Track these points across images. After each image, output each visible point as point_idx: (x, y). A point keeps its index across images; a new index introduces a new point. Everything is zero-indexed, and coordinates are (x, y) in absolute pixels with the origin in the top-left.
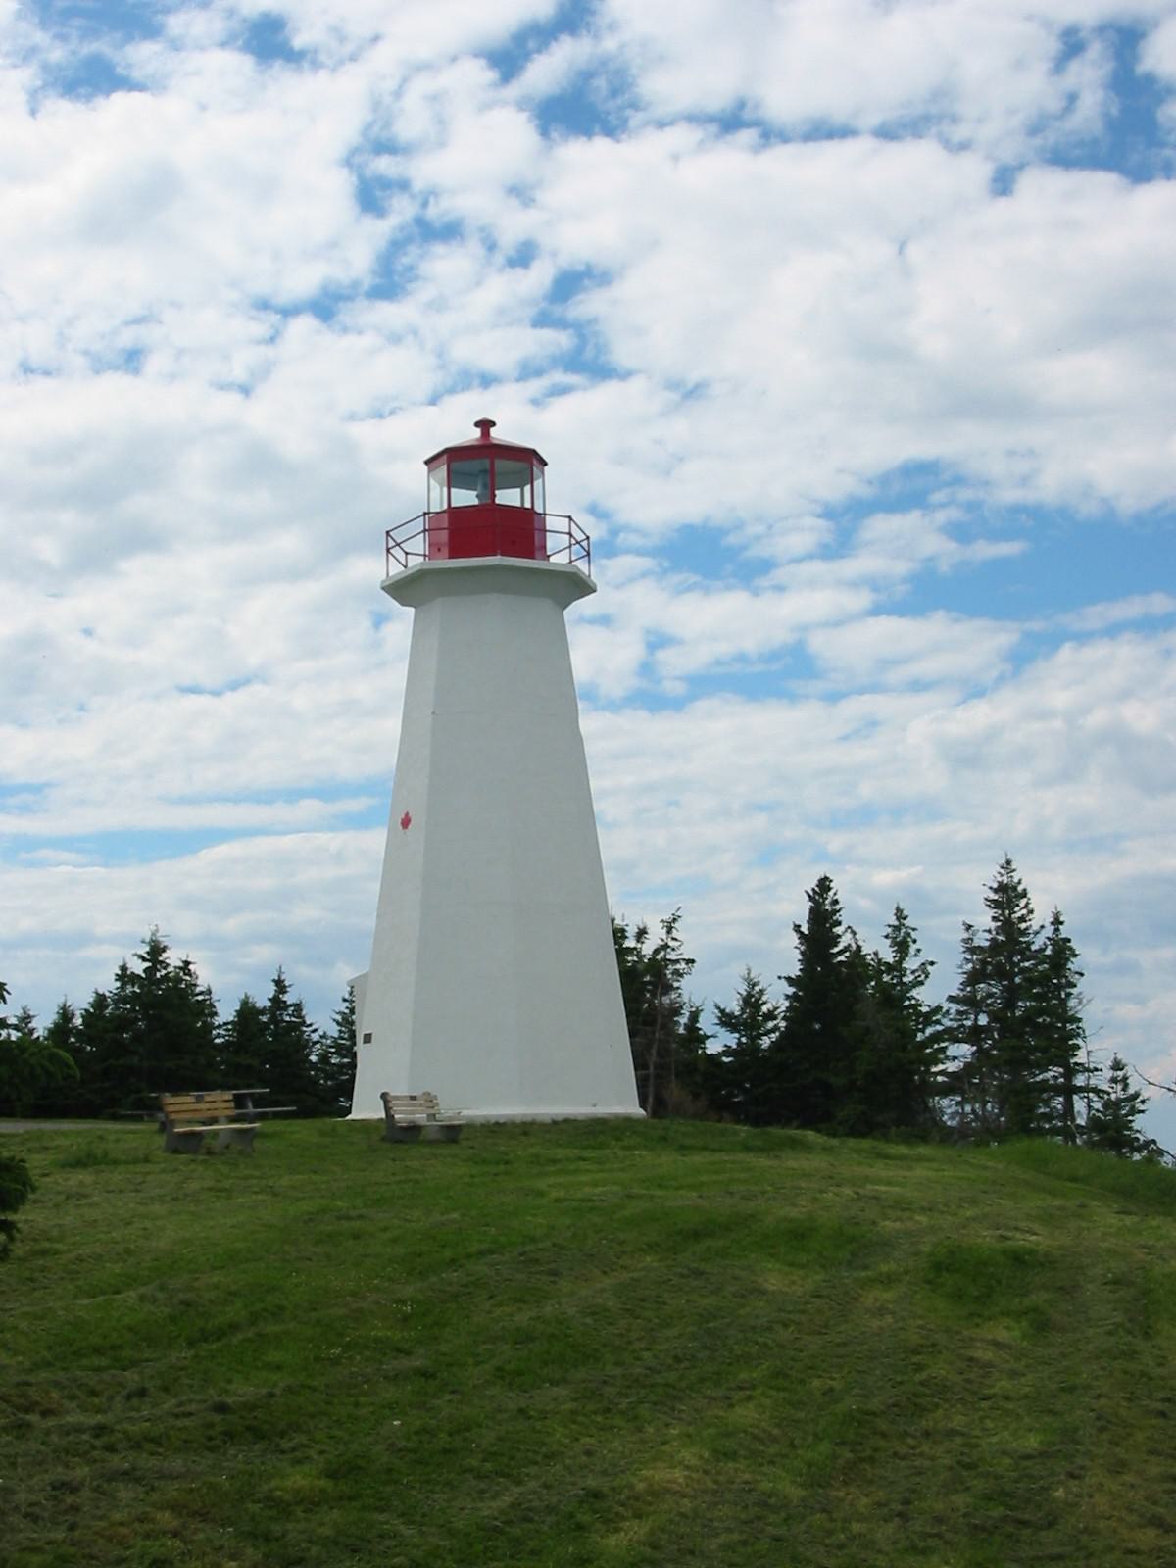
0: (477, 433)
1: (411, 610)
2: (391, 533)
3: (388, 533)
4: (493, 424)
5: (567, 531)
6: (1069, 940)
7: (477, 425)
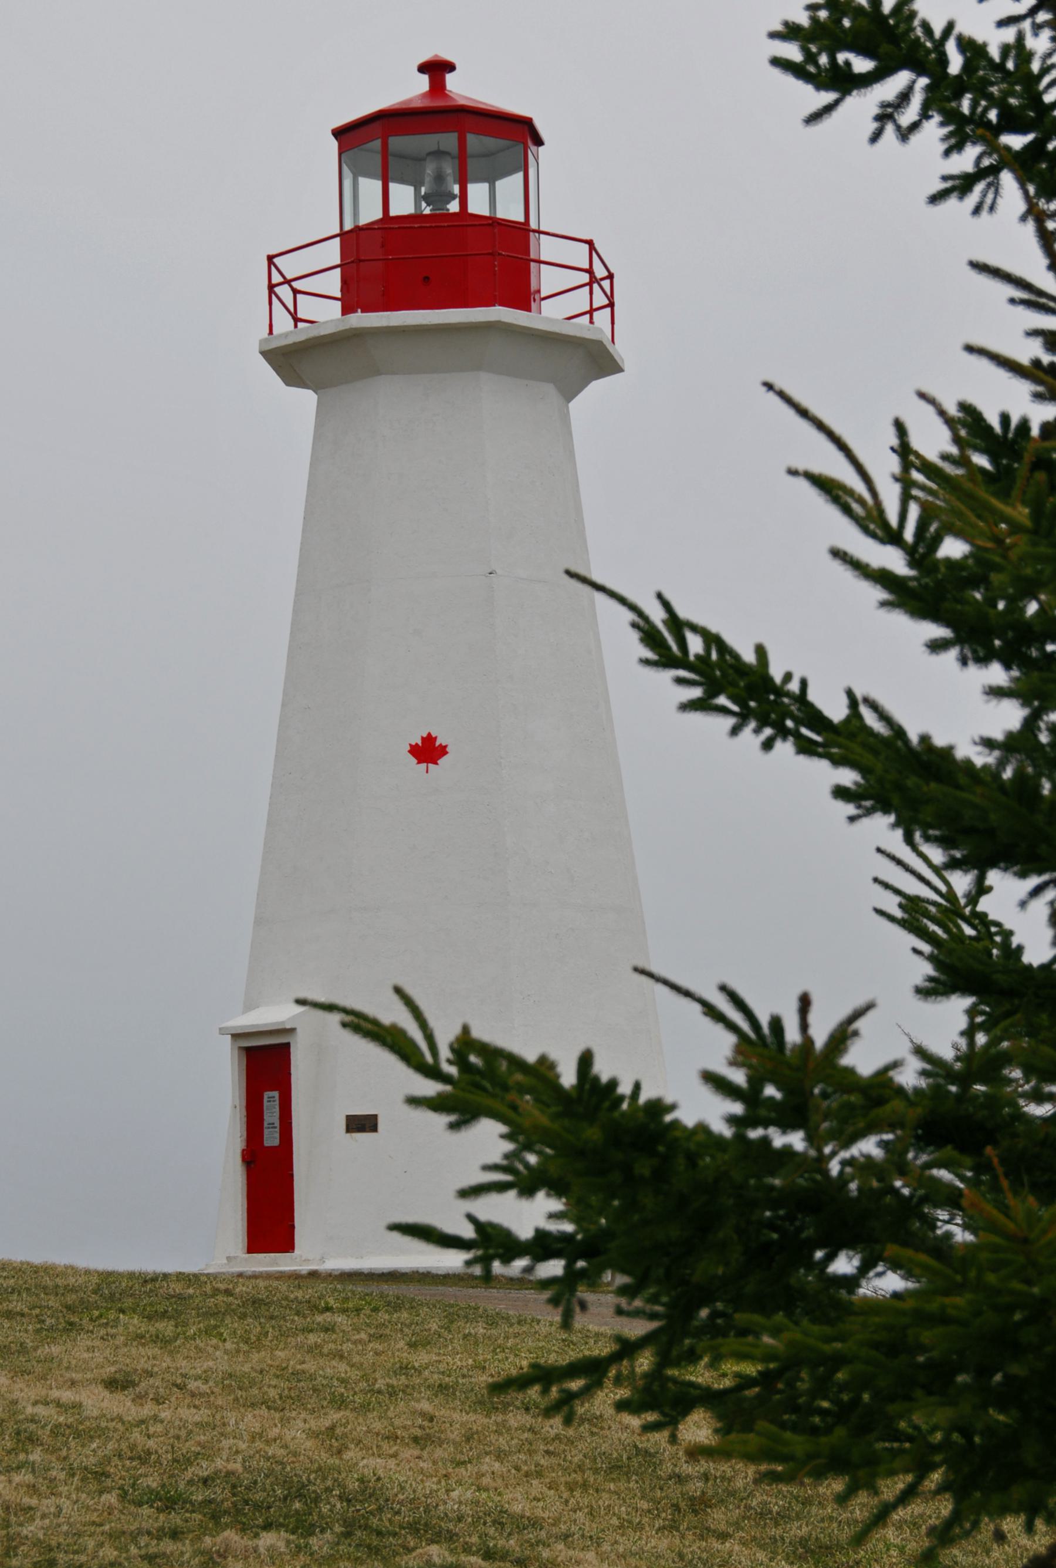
0: (423, 83)
1: (307, 398)
2: (276, 260)
3: (270, 259)
4: (450, 67)
5: (586, 266)
6: (454, 1126)
7: (423, 68)
